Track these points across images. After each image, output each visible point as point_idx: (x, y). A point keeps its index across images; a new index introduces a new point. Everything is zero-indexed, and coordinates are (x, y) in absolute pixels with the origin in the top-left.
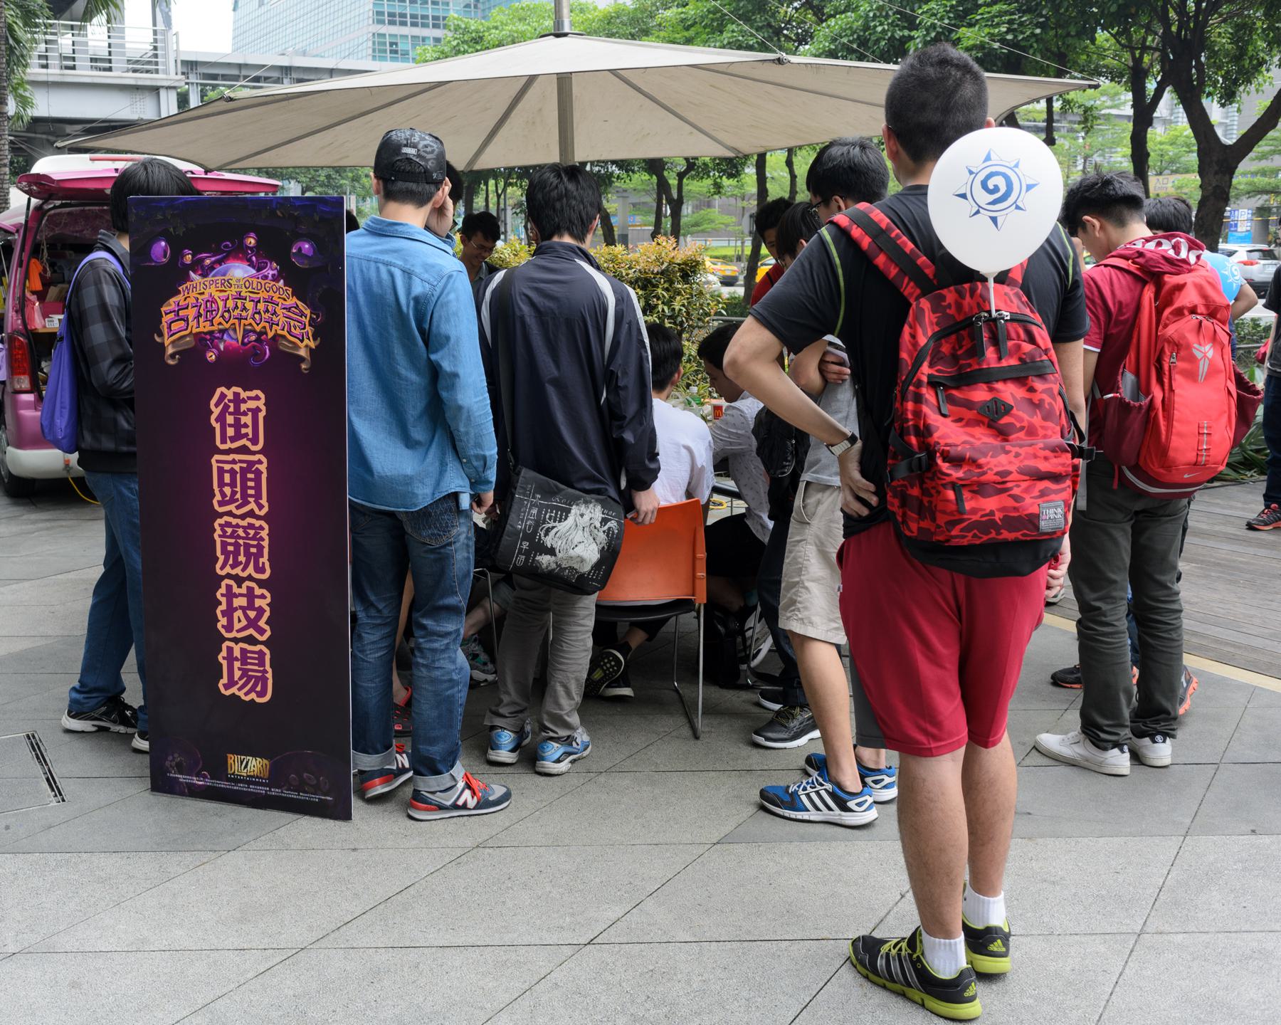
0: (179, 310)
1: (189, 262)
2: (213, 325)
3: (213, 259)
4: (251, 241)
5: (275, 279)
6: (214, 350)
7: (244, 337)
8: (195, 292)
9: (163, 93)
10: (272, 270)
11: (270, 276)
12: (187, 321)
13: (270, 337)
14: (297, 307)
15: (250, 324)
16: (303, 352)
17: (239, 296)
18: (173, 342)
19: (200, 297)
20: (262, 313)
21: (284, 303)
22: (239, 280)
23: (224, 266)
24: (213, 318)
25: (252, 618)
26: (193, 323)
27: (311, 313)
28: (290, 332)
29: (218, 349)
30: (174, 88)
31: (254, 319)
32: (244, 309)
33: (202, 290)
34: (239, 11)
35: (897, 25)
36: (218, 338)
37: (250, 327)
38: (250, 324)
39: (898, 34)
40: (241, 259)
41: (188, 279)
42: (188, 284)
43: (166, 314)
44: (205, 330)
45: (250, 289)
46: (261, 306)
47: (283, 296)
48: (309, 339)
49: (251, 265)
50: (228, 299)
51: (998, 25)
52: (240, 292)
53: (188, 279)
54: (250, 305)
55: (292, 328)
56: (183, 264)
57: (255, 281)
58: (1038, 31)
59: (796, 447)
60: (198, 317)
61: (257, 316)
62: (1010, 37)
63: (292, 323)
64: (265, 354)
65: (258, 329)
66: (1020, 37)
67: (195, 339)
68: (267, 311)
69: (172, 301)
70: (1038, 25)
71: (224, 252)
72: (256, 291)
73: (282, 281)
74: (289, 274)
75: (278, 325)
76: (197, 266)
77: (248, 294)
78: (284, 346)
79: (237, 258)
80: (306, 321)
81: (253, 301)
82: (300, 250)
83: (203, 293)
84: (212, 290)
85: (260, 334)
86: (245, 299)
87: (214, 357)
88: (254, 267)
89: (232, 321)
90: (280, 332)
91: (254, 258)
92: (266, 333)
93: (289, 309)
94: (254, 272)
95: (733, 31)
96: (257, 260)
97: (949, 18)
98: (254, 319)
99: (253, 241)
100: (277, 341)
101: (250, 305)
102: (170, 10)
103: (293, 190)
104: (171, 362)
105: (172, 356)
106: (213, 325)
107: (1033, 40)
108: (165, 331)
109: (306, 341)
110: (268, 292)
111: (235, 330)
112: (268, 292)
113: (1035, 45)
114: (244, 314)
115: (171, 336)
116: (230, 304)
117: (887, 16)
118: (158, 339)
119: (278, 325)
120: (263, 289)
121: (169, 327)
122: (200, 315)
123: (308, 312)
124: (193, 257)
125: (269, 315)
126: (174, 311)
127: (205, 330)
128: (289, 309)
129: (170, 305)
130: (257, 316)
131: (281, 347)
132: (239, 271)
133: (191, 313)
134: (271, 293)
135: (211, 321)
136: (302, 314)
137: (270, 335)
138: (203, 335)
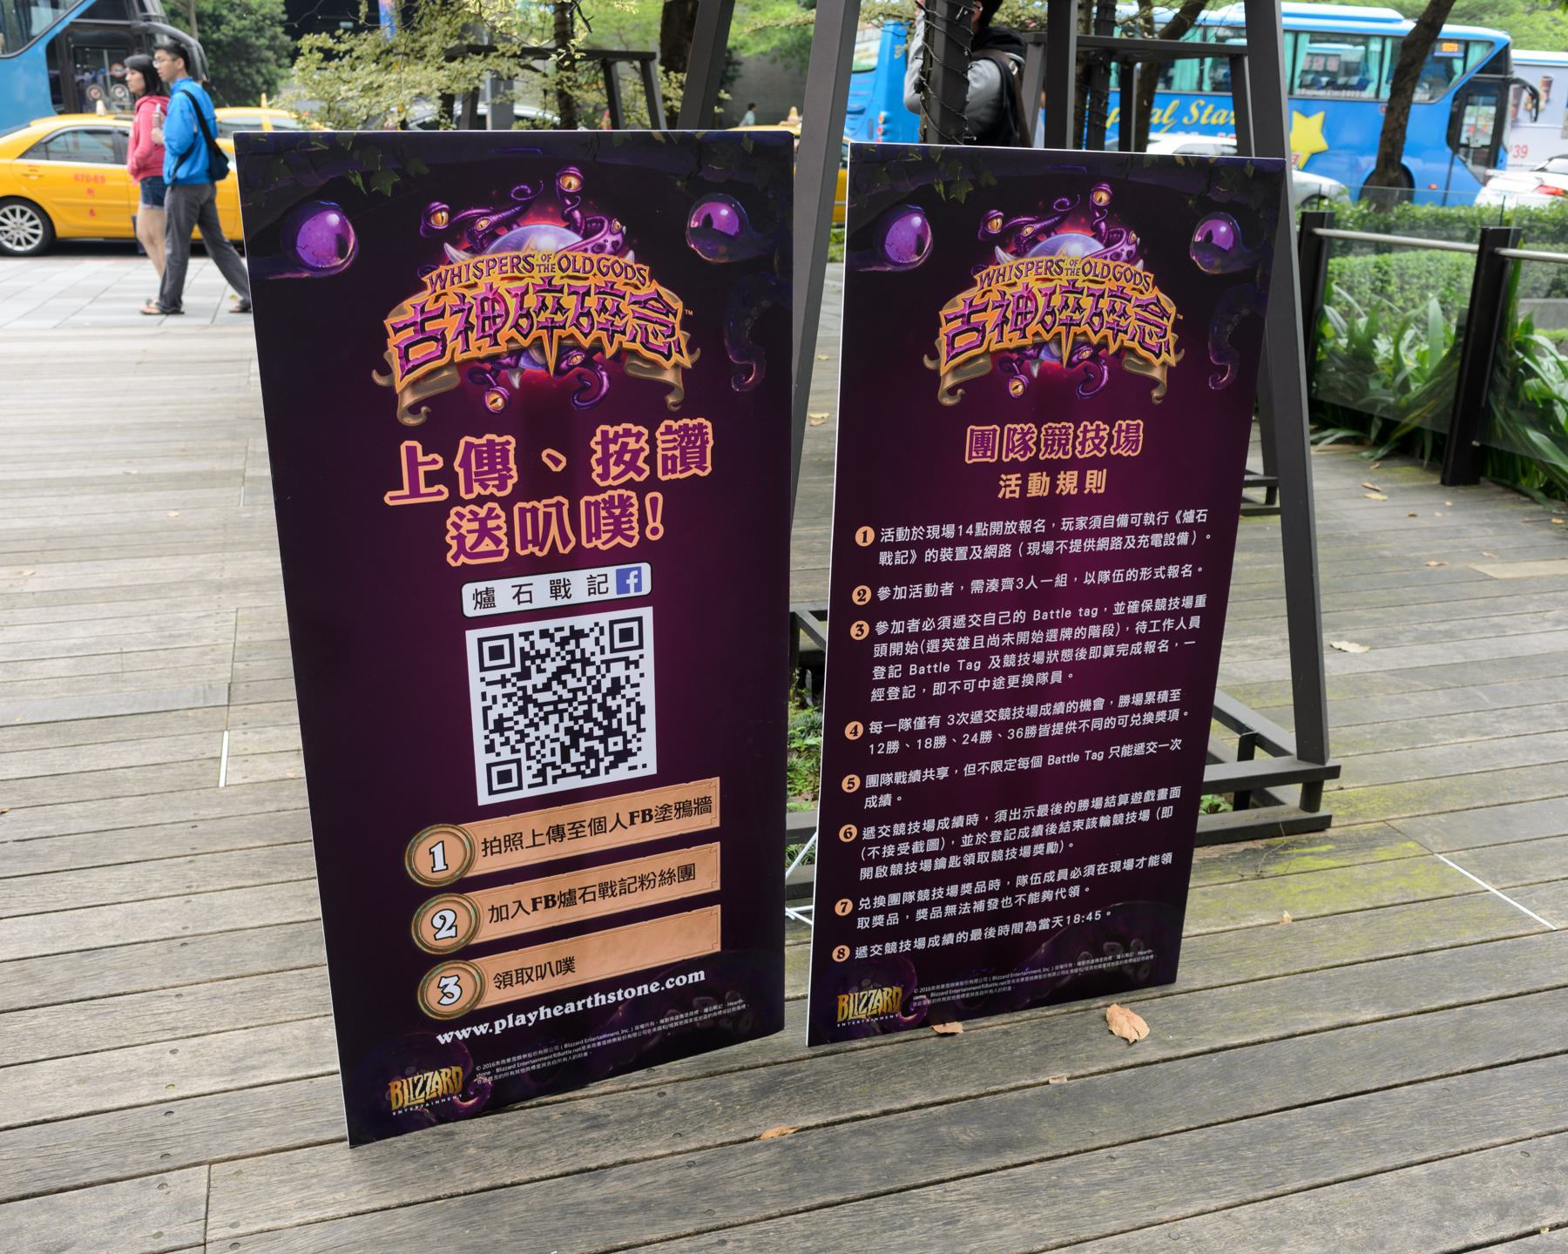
0: (970, 314)
1: (442, 227)
2: (496, 344)
3: (1038, 226)
5: (618, 250)
6: (500, 389)
7: (559, 360)
8: (456, 285)
10: (1129, 244)
11: (609, 245)
12: (440, 338)
13: (1111, 352)
14: (659, 298)
15: (1085, 333)
16: (1157, 373)
17: (548, 286)
18: (955, 369)
19: (1009, 291)
20: (595, 314)
21: (636, 292)
22: (548, 257)
23: (517, 230)
24: (498, 330)
25: (718, 779)
26: (991, 335)
27: (685, 307)
28: (646, 344)
29: (509, 386)
31: (1091, 323)
32: (560, 308)
33: (473, 280)
36: (508, 366)
37: (570, 342)
38: (572, 336)
40: (553, 218)
41: (993, 260)
42: (442, 269)
43: (396, 331)
44: (1011, 346)
45: (570, 272)
46: (1104, 304)
48: (680, 352)
50: (526, 292)
52: (1075, 281)
53: (993, 260)
55: (651, 336)
56: (987, 234)
57: (580, 256)
59: (1555, 427)
60: (466, 330)
61: (584, 321)
63: (650, 327)
64: (601, 385)
67: (460, 374)
68: (603, 309)
69: (959, 298)
71: (517, 204)
72: (580, 275)
73: (631, 254)
75: (623, 333)
76: (462, 233)
77: (1087, 284)
78: (1130, 365)
81: (576, 293)
83: (475, 285)
84: (495, 279)
86: (1081, 293)
87: (500, 401)
88: (577, 231)
89: (535, 333)
90: (1128, 344)
91: (577, 214)
92: (601, 350)
93: (1144, 307)
96: (1107, 228)
98: (1091, 323)
99: (574, 182)
100: (622, 361)
101: (1087, 302)
103: (1043, 96)
104: (948, 401)
105: (952, 391)
106: (496, 344)
108: (396, 364)
109: (676, 357)
110: (1117, 280)
111: (1059, 344)
112: (604, 275)
114: (559, 318)
115: (409, 371)
116: (531, 301)
118: (929, 364)
119: (623, 333)
120: (595, 270)
121: (951, 344)
122: (469, 327)
124: (451, 216)
125: (607, 316)
126: (414, 324)
127: (481, 354)
128: (643, 303)
129: (403, 312)
130: (584, 321)
131: (1127, 367)
132: (1077, 246)
133: (451, 324)
134: (611, 277)
135: (1023, 331)
136: (669, 310)
137: (610, 351)
138: (1007, 354)
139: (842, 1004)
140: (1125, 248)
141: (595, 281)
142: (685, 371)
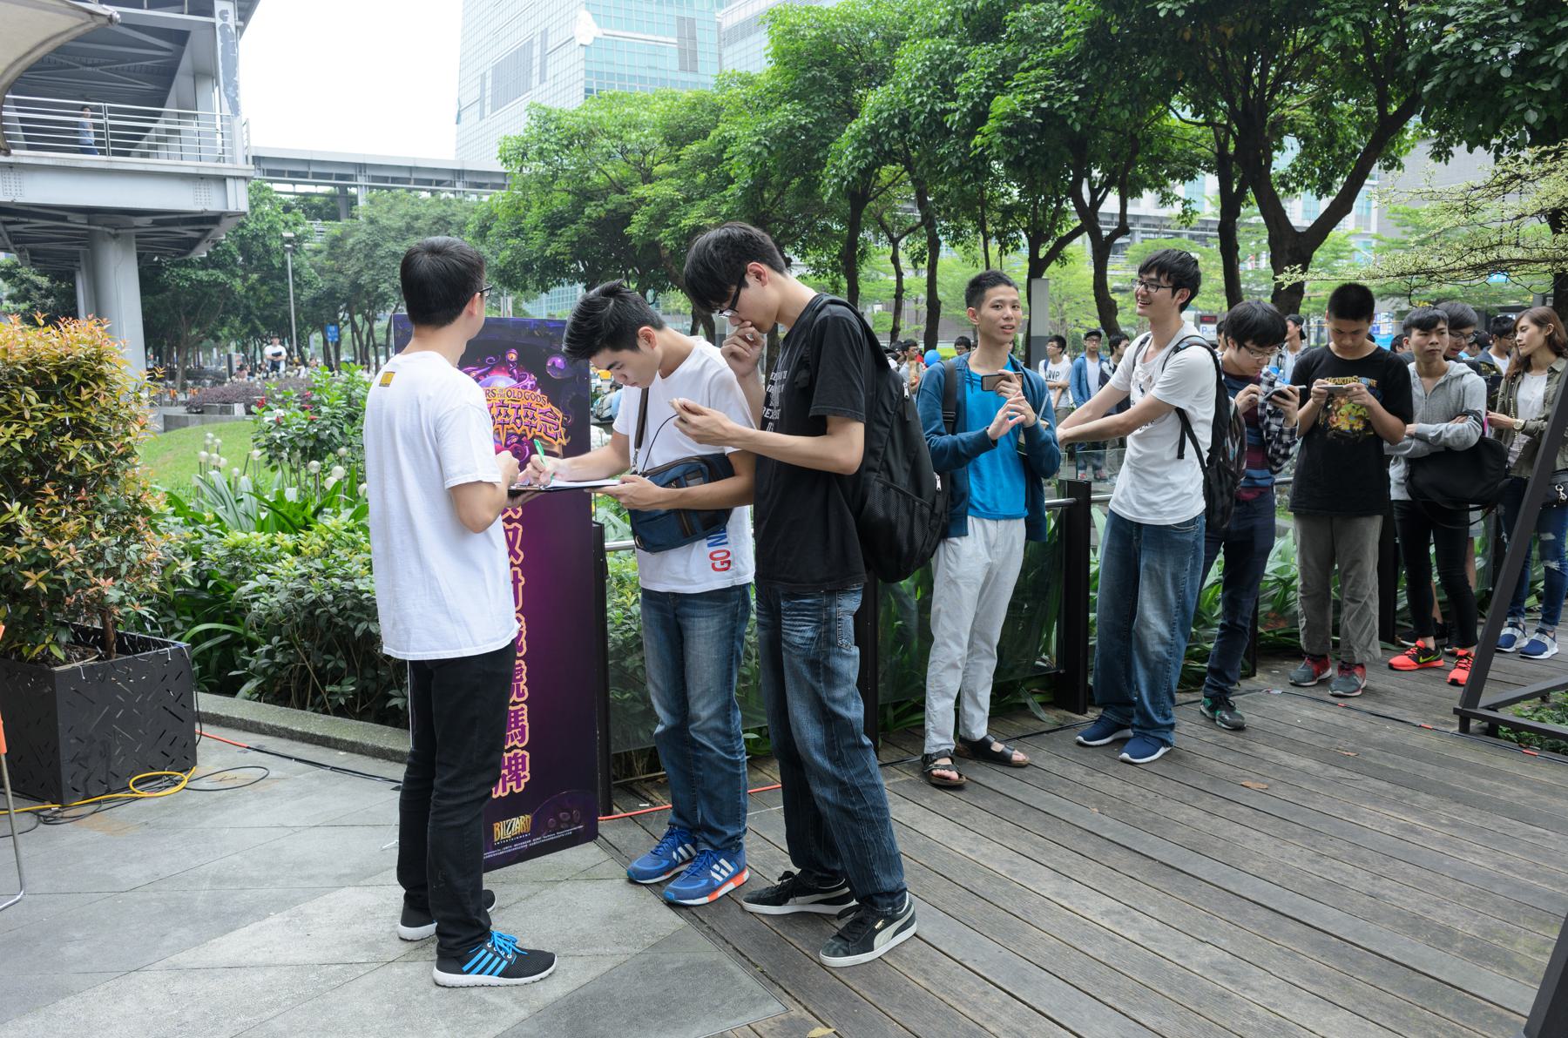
4: (513, 356)
5: (533, 388)
9: (230, 183)
14: (552, 411)
23: (488, 378)
30: (245, 178)
31: (515, 423)
34: (462, 123)
35: (939, 97)
39: (939, 107)
46: (521, 412)
47: (541, 403)
49: (513, 376)
51: (1034, 91)
54: (512, 412)
58: (1076, 98)
62: (1044, 105)
65: (519, 432)
66: (1057, 105)
68: (527, 416)
70: (1078, 92)
74: (549, 387)
79: (500, 371)
80: (559, 423)
82: (554, 364)
85: (521, 436)
93: (545, 414)
94: (515, 382)
95: (786, 110)
97: (987, 87)
98: (515, 423)
101: (512, 412)
102: (237, 95)
107: (1072, 108)
109: (559, 440)
113: (1074, 114)
114: (507, 419)
117: (928, 86)
123: (560, 415)
128: (545, 414)
136: (556, 417)
137: (530, 436)
139: (496, 829)
140: (529, 383)
141: (523, 402)
142: (563, 447)
